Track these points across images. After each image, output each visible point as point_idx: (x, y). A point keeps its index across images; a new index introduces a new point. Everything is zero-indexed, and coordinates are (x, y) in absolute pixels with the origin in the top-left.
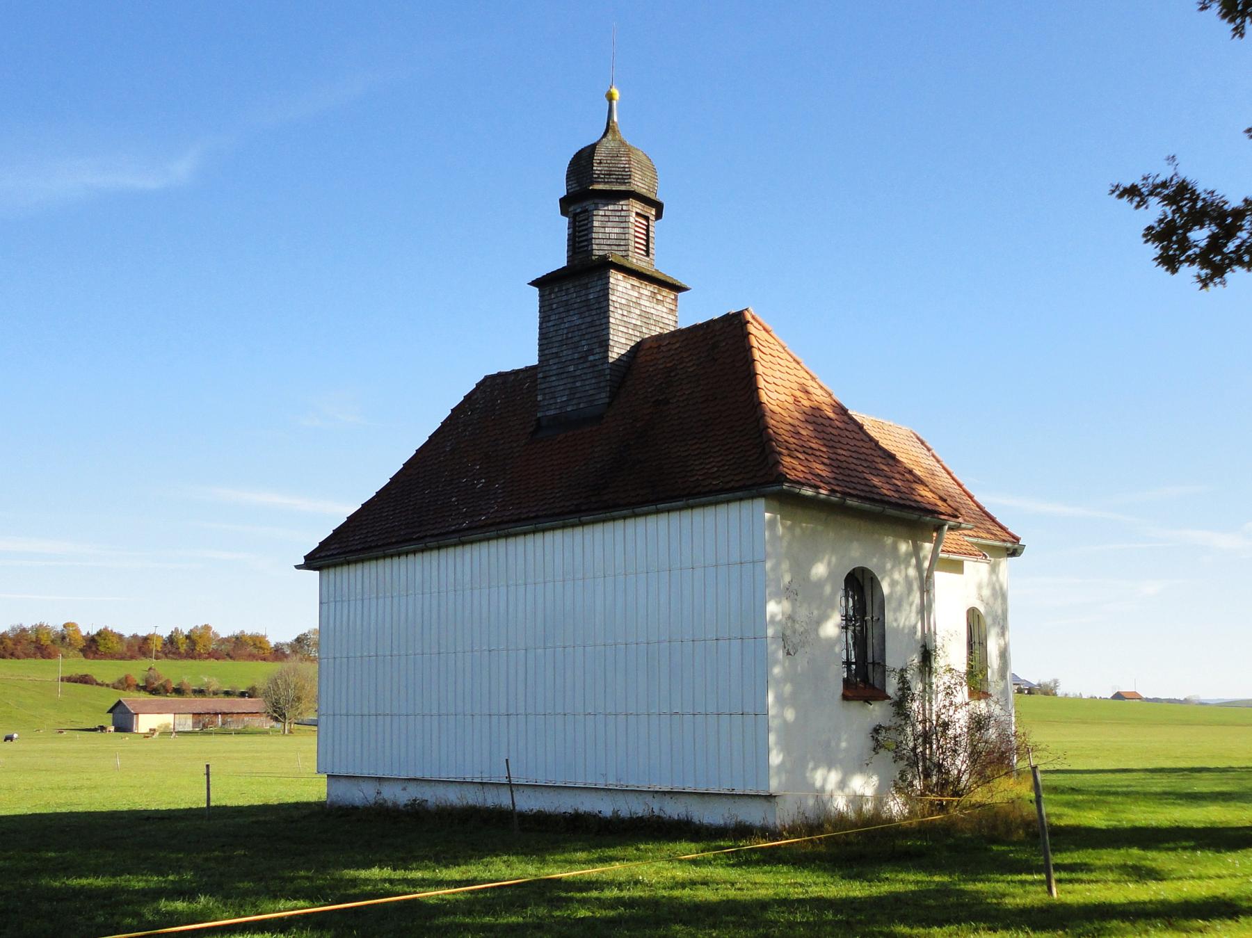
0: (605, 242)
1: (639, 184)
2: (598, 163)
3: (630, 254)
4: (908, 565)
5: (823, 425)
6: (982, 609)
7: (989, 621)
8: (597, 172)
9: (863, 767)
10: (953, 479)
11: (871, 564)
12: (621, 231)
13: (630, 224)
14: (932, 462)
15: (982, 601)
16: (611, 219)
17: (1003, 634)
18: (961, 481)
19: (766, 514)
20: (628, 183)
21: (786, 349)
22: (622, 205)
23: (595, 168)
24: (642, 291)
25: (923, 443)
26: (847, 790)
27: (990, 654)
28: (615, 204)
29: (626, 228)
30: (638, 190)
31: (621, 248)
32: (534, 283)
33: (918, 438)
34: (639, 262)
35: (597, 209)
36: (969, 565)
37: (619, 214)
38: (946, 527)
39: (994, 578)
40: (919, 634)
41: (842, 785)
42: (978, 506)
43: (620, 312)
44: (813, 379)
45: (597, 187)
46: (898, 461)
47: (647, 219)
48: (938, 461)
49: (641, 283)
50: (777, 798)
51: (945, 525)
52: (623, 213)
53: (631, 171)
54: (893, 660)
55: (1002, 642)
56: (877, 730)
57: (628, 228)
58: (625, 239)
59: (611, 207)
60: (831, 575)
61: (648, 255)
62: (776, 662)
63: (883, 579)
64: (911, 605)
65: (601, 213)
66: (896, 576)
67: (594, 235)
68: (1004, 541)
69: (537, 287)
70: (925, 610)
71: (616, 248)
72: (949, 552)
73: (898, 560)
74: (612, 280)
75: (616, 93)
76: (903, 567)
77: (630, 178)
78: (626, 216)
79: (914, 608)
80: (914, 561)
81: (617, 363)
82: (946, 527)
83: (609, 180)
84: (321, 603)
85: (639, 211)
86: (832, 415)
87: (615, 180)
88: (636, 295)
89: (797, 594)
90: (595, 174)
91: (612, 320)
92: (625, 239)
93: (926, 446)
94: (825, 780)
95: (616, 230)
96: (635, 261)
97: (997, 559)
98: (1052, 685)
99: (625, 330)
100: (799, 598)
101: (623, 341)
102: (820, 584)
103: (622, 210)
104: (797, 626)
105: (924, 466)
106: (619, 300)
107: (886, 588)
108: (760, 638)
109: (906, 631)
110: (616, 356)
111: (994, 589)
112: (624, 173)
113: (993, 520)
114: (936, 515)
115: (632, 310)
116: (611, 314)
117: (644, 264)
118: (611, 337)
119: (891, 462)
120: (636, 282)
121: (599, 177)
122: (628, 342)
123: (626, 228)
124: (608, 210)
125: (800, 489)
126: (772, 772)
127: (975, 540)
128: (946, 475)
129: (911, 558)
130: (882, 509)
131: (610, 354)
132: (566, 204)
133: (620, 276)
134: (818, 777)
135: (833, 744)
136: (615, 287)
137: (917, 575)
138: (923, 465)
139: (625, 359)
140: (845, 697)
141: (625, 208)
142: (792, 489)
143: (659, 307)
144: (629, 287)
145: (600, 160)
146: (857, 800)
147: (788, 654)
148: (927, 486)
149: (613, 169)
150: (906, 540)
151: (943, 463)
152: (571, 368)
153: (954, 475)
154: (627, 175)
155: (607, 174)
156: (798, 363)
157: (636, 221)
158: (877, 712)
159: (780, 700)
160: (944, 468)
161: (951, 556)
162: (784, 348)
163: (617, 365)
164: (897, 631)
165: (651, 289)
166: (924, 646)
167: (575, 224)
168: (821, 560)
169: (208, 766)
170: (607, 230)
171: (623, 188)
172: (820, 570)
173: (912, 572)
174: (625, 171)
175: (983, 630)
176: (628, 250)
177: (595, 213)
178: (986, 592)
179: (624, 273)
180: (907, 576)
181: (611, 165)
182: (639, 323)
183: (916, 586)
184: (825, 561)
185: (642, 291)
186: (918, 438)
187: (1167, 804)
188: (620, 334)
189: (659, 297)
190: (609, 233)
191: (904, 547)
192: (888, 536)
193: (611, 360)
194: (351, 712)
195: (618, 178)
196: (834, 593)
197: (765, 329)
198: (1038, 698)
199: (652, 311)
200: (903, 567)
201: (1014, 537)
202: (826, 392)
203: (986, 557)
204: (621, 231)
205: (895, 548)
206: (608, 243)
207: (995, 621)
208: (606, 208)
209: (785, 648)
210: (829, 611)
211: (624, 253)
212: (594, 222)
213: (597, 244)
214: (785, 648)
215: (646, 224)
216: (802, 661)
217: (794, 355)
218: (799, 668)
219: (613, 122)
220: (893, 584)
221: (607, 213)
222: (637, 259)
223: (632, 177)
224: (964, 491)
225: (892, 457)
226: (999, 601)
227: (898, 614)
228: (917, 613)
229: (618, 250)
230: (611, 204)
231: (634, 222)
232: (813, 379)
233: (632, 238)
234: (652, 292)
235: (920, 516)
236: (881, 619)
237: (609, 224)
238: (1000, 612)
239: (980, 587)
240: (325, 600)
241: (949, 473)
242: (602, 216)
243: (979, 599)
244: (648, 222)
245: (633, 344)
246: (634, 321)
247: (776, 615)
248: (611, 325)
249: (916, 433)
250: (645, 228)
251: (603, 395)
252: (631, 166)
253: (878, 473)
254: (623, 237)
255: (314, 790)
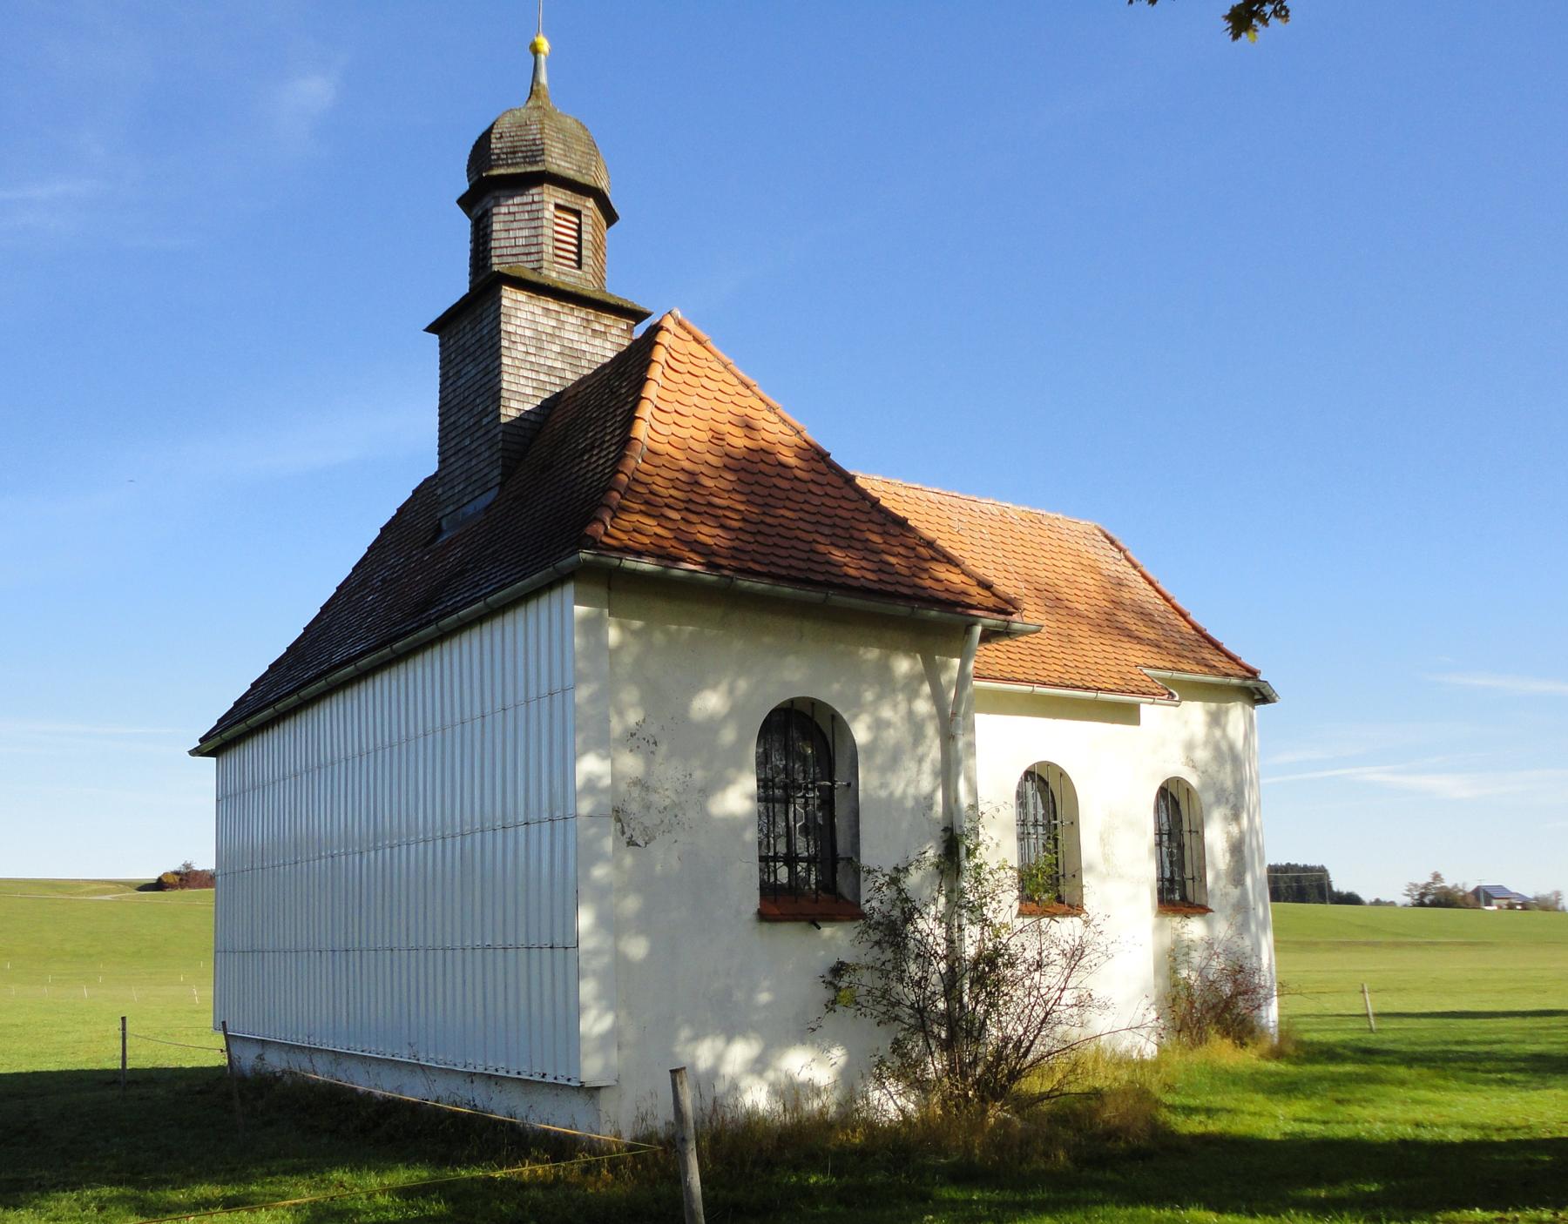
0: (509, 251)
1: (558, 161)
2: (496, 138)
3: (545, 264)
4: (913, 695)
5: (745, 471)
6: (1193, 780)
7: (1207, 797)
8: (496, 151)
9: (808, 1033)
10: (1158, 591)
11: (829, 692)
12: (533, 232)
13: (545, 221)
14: (1124, 568)
15: (1193, 767)
16: (518, 217)
17: (1236, 817)
18: (1169, 594)
19: (575, 607)
20: (541, 161)
21: (729, 366)
22: (533, 195)
23: (493, 146)
24: (562, 317)
25: (1112, 542)
26: (771, 1075)
27: (1211, 848)
28: (522, 195)
29: (538, 227)
30: (554, 169)
31: (532, 258)
32: (430, 329)
33: (1106, 537)
34: (563, 277)
35: (499, 205)
36: (1148, 711)
37: (528, 208)
38: (978, 630)
39: (1218, 733)
40: (938, 809)
41: (759, 1066)
42: (1195, 628)
43: (523, 348)
44: (771, 409)
45: (495, 172)
46: (912, 529)
47: (578, 214)
48: (1135, 566)
49: (563, 306)
50: (602, 1091)
51: (975, 624)
52: (534, 207)
53: (543, 144)
54: (876, 852)
55: (1234, 829)
56: (839, 970)
57: (542, 227)
58: (537, 244)
59: (517, 200)
60: (736, 711)
61: (580, 267)
62: (597, 857)
63: (855, 717)
64: (920, 760)
65: (504, 210)
66: (887, 713)
67: (494, 244)
68: (1227, 675)
69: (436, 333)
70: (948, 771)
71: (524, 258)
72: (1154, 694)
73: (885, 682)
74: (505, 302)
75: (544, 45)
76: (900, 697)
77: (543, 154)
78: (538, 211)
79: (927, 767)
80: (926, 689)
81: (516, 423)
82: (978, 630)
83: (514, 161)
84: (217, 800)
85: (560, 202)
86: (792, 461)
87: (522, 160)
88: (554, 323)
89: (655, 743)
90: (493, 154)
91: (505, 360)
92: (537, 244)
93: (1117, 547)
94: (720, 1058)
95: (526, 233)
96: (554, 275)
97: (1224, 705)
98: (1553, 898)
99: (534, 375)
100: (663, 749)
101: (529, 391)
102: (712, 725)
103: (533, 202)
104: (655, 798)
105: (1105, 572)
106: (520, 331)
107: (861, 733)
108: (559, 817)
109: (910, 803)
110: (514, 414)
111: (1217, 748)
112: (534, 148)
113: (1217, 646)
114: (959, 609)
115: (546, 345)
116: (504, 351)
117: (572, 280)
118: (504, 385)
119: (895, 530)
120: (553, 305)
121: (499, 159)
122: (537, 393)
123: (538, 227)
124: (514, 205)
125: (621, 559)
126: (584, 1047)
127: (1168, 674)
128: (1144, 584)
129: (922, 682)
130: (822, 596)
131: (503, 411)
132: (466, 202)
133: (521, 296)
134: (704, 1054)
135: (739, 995)
136: (513, 312)
137: (934, 710)
138: (1104, 572)
139: (532, 417)
140: (763, 916)
141: (536, 198)
142: (603, 559)
143: (598, 342)
144: (539, 311)
145: (501, 133)
146: (791, 1093)
147: (631, 843)
148: (957, 565)
149: (518, 144)
150: (908, 651)
151: (1144, 569)
152: (467, 442)
153: (1159, 585)
154: (538, 150)
155: (511, 153)
156: (748, 387)
157: (557, 217)
158: (836, 939)
159: (609, 923)
160: (1144, 576)
161: (1036, 689)
162: (725, 367)
163: (515, 426)
164: (891, 805)
165: (583, 315)
166: (949, 830)
167: (478, 234)
168: (714, 687)
169: (123, 1019)
170: (512, 234)
171: (535, 168)
172: (711, 702)
173: (923, 706)
174: (535, 145)
175: (1197, 807)
176: (542, 259)
177: (495, 210)
178: (1202, 755)
179: (528, 291)
180: (911, 713)
181: (515, 139)
182: (558, 365)
183: (931, 730)
184: (724, 687)
185: (562, 317)
186: (1106, 537)
187: (1487, 1082)
188: (523, 381)
189: (597, 327)
190: (515, 238)
191: (903, 665)
192: (866, 645)
193: (504, 420)
194: (511, 941)
195: (527, 157)
196: (741, 742)
197: (696, 339)
198: (1537, 914)
199: (584, 347)
200: (900, 697)
201: (1248, 670)
202: (792, 427)
203: (1173, 696)
204: (533, 232)
205: (884, 670)
206: (514, 253)
207: (1221, 797)
208: (510, 202)
209: (623, 833)
210: (731, 772)
211: (535, 265)
212: (494, 225)
213: (498, 256)
214: (623, 833)
215: (577, 221)
216: (664, 856)
217: (741, 374)
218: (658, 868)
219: (538, 84)
220: (879, 725)
221: (512, 209)
222: (558, 272)
223: (546, 152)
224: (1174, 607)
225: (902, 523)
226: (1228, 768)
227: (889, 775)
228: (935, 774)
229: (527, 262)
230: (518, 195)
231: (552, 217)
232: (771, 409)
233: (550, 241)
234: (583, 319)
235: (913, 608)
236: (853, 784)
237: (515, 225)
238: (1229, 784)
239: (1190, 746)
240: (220, 797)
241: (1151, 583)
242: (505, 214)
243: (1187, 764)
244: (580, 219)
245: (547, 395)
246: (549, 363)
247: (600, 778)
248: (504, 368)
249: (1104, 529)
250: (574, 227)
251: (496, 472)
252: (544, 135)
253: (849, 540)
254: (534, 241)
255: (208, 1052)
